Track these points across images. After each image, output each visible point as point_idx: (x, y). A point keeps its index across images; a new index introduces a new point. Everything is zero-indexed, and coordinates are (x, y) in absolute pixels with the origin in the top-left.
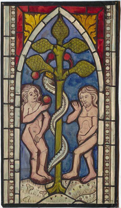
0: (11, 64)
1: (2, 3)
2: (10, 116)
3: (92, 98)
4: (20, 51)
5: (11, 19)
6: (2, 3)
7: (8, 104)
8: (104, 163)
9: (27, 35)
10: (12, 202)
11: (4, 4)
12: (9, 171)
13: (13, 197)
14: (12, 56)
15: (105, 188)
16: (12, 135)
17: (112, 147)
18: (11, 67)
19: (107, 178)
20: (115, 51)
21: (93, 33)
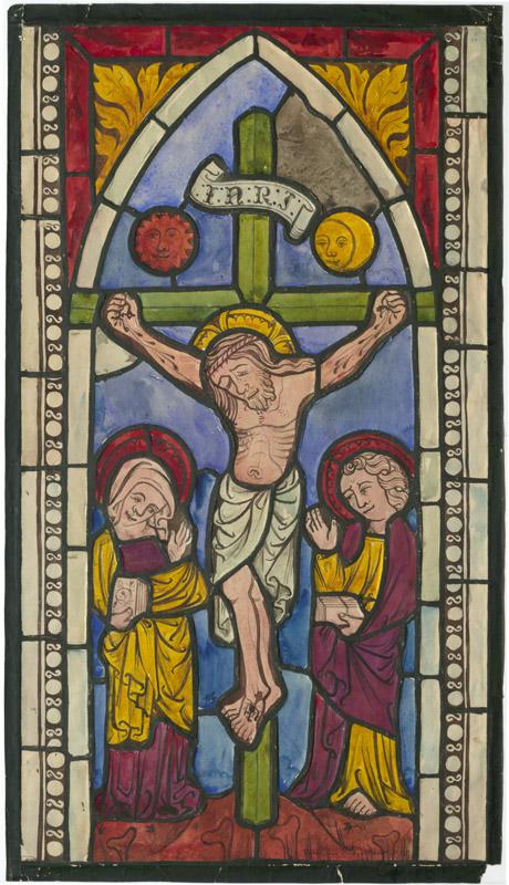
1: (8, 879)
2: (46, 830)
3: (396, 614)
6: (8, 879)
10: (55, 849)
13: (59, 583)
15: (448, 484)
16: (55, 490)
17: (474, 123)
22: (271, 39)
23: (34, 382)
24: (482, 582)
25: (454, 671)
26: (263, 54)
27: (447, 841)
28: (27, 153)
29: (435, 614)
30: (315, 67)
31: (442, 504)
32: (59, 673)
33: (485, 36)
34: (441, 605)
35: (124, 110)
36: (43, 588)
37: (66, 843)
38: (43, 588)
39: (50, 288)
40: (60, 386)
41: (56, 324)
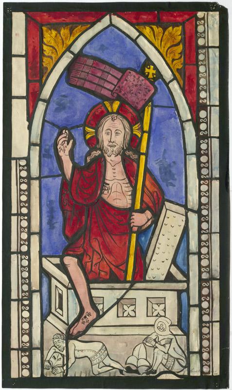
0: (209, 198)
1: (3, 387)
4: (188, 100)
5: (209, 187)
6: (3, 387)
8: (28, 201)
10: (26, 373)
12: (20, 283)
13: (26, 229)
14: (203, 47)
18: (209, 255)
22: (119, 16)
24: (217, 322)
25: (204, 250)
26: (114, 22)
27: (202, 207)
28: (14, 253)
30: (137, 27)
31: (199, 254)
32: (28, 366)
33: (218, 111)
34: (200, 353)
36: (20, 270)
37: (30, 370)
38: (20, 283)
39: (24, 367)
40: (27, 205)
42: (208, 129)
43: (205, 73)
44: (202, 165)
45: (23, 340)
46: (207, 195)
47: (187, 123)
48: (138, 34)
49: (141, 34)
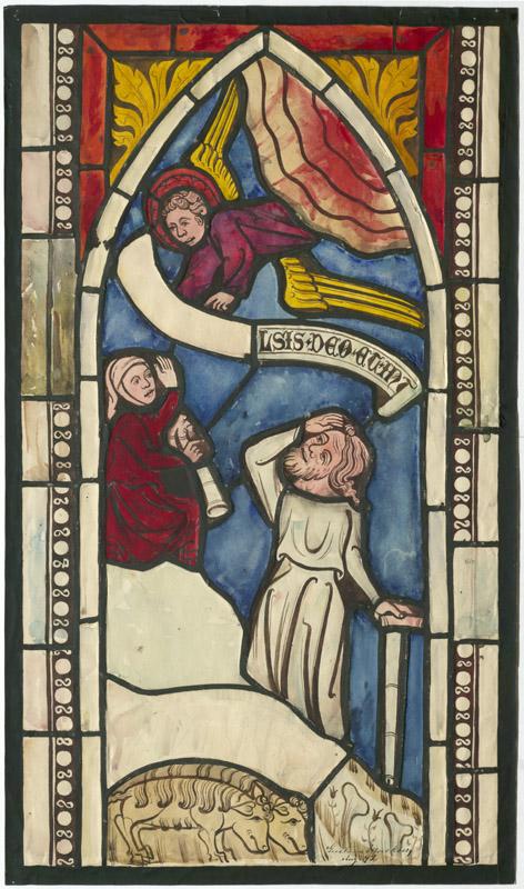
1: (9, 11)
6: (9, 11)
7: (46, 647)
9: (126, 143)
11: (17, 18)
12: (51, 626)
19: (464, 398)
20: (494, 764)
21: (405, 124)
23: (43, 244)
26: (273, 49)
29: (442, 515)
35: (141, 117)
38: (51, 626)
39: (60, 172)
41: (68, 55)
42: (475, 404)
43: (467, 521)
44: (458, 469)
45: (57, 700)
46: (470, 362)
47: (437, 503)
48: (329, 79)
49: (336, 79)
